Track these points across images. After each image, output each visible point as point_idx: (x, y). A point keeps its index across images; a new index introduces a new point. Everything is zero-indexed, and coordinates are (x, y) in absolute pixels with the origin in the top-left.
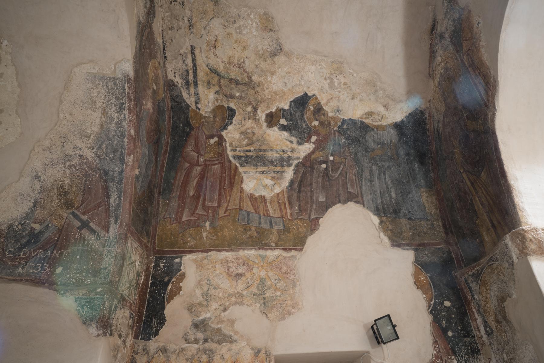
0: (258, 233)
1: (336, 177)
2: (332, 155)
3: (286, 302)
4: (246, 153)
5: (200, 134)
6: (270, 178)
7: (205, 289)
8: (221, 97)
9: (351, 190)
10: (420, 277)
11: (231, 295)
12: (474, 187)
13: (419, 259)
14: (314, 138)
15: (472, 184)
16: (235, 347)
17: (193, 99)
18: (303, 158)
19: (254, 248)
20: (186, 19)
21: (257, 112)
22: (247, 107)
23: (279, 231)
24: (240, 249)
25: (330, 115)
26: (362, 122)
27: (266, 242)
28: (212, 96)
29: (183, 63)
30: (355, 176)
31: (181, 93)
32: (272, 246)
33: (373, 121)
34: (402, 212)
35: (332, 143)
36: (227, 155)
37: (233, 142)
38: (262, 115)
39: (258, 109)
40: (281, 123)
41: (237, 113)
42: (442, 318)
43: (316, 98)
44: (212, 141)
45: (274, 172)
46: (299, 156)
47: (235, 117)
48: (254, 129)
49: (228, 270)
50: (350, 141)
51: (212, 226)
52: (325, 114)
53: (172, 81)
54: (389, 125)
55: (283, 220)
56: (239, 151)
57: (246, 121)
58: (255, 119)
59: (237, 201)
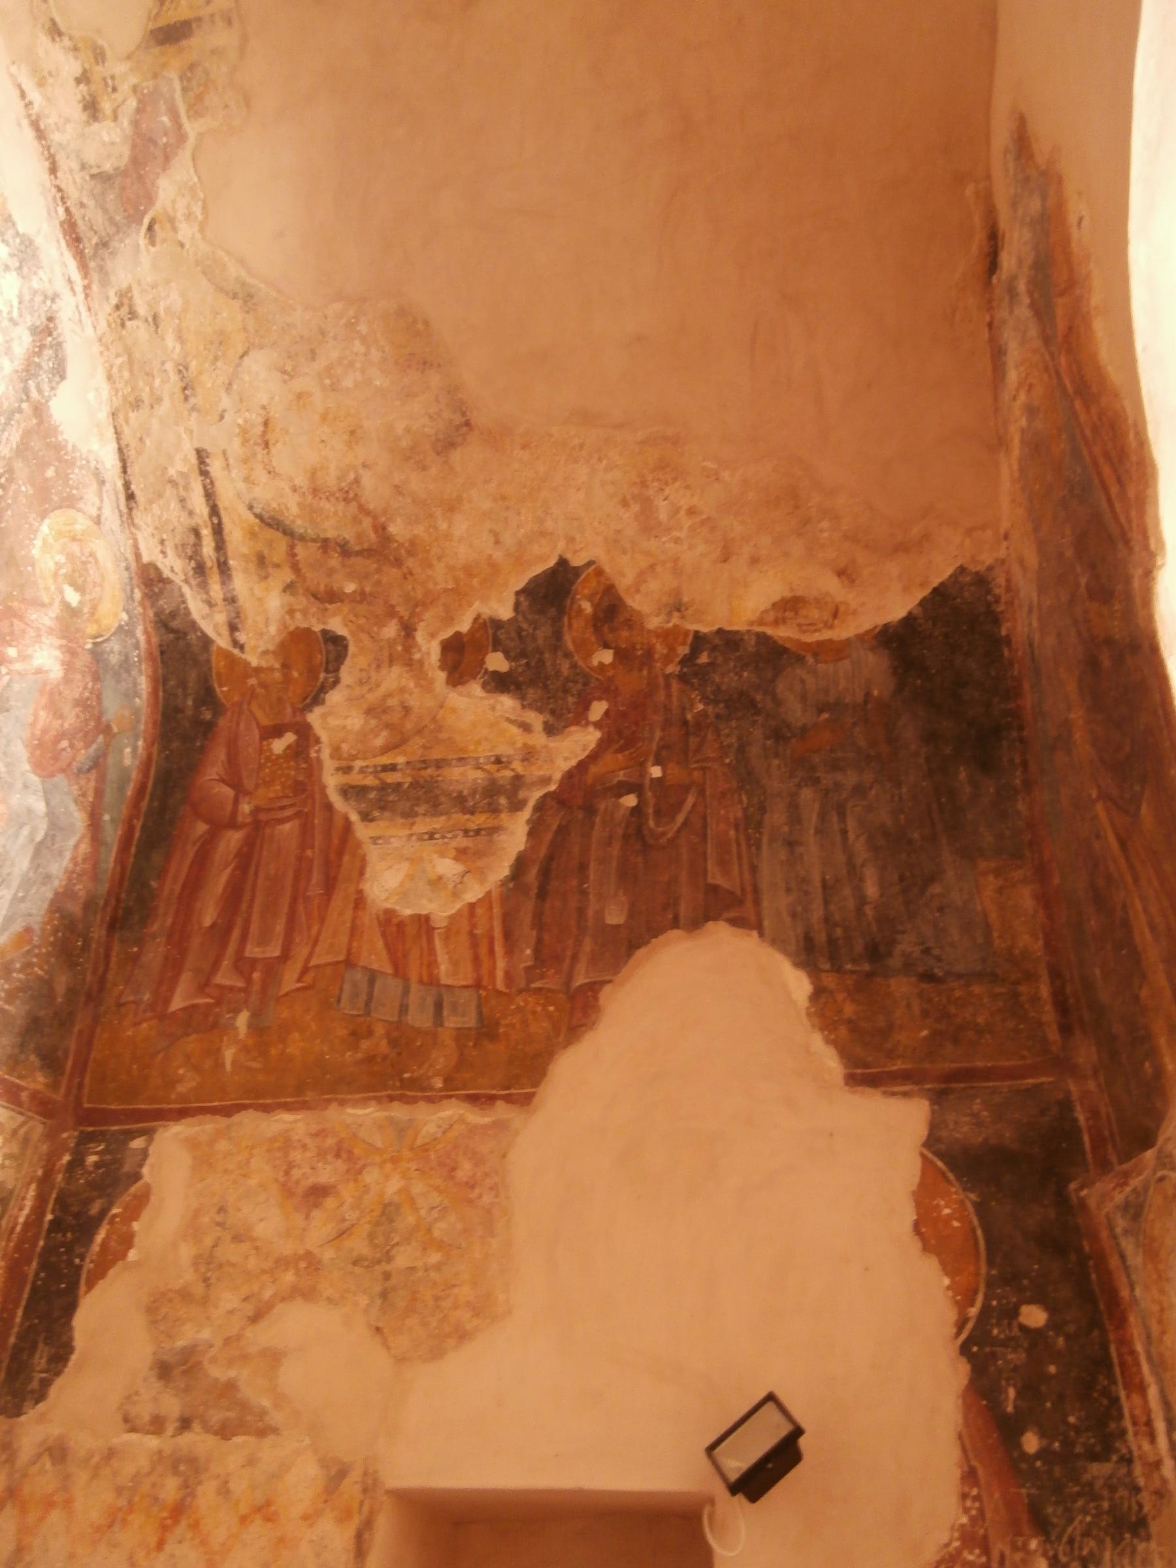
0: (393, 1042)
1: (670, 835)
2: (657, 762)
3: (456, 1290)
4: (382, 775)
5: (242, 726)
6: (453, 853)
7: (209, 1241)
8: (301, 601)
9: (716, 878)
10: (938, 1206)
11: (283, 1263)
12: (1128, 859)
13: (944, 1133)
14: (598, 709)
15: (1123, 843)
16: (269, 1452)
17: (221, 618)
18: (563, 778)
19: (374, 1098)
20: (169, 366)
21: (414, 638)
22: (381, 624)
23: (461, 1035)
24: (329, 1101)
25: (654, 623)
26: (763, 639)
27: (416, 1074)
28: (275, 602)
29: (179, 506)
30: (737, 828)
31: (184, 602)
32: (432, 1089)
33: (805, 628)
34: (898, 949)
35: (658, 718)
36: (323, 788)
37: (343, 741)
38: (430, 648)
39: (415, 630)
40: (491, 668)
41: (352, 649)
42: (1005, 1376)
43: (599, 572)
44: (278, 746)
45: (466, 832)
46: (548, 773)
47: (348, 662)
48: (407, 696)
49: (287, 1173)
50: (722, 705)
51: (256, 1029)
52: (633, 622)
53: (157, 569)
54: (860, 637)
55: (479, 997)
56: (362, 770)
57: (384, 671)
58: (409, 663)
59: (344, 939)
